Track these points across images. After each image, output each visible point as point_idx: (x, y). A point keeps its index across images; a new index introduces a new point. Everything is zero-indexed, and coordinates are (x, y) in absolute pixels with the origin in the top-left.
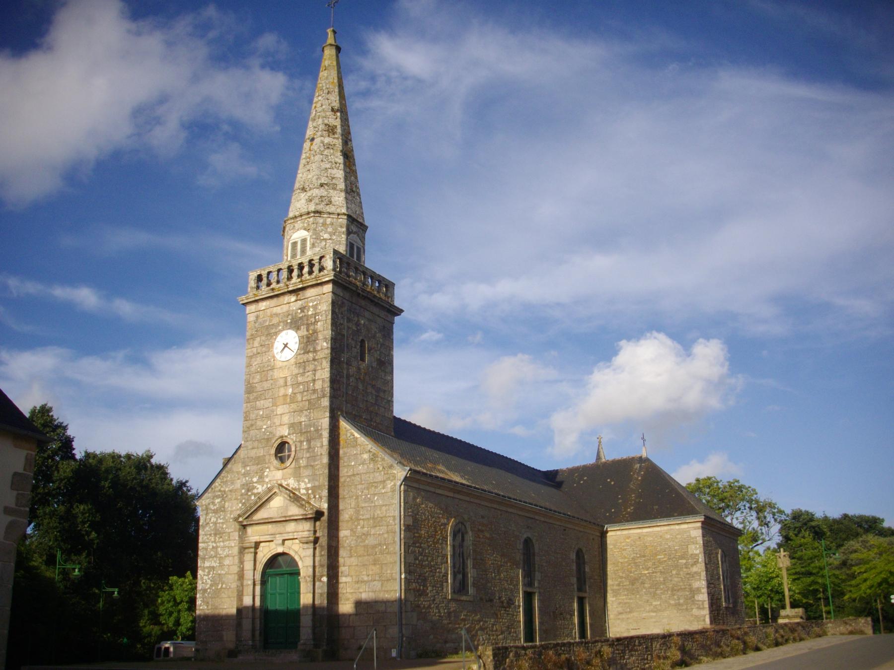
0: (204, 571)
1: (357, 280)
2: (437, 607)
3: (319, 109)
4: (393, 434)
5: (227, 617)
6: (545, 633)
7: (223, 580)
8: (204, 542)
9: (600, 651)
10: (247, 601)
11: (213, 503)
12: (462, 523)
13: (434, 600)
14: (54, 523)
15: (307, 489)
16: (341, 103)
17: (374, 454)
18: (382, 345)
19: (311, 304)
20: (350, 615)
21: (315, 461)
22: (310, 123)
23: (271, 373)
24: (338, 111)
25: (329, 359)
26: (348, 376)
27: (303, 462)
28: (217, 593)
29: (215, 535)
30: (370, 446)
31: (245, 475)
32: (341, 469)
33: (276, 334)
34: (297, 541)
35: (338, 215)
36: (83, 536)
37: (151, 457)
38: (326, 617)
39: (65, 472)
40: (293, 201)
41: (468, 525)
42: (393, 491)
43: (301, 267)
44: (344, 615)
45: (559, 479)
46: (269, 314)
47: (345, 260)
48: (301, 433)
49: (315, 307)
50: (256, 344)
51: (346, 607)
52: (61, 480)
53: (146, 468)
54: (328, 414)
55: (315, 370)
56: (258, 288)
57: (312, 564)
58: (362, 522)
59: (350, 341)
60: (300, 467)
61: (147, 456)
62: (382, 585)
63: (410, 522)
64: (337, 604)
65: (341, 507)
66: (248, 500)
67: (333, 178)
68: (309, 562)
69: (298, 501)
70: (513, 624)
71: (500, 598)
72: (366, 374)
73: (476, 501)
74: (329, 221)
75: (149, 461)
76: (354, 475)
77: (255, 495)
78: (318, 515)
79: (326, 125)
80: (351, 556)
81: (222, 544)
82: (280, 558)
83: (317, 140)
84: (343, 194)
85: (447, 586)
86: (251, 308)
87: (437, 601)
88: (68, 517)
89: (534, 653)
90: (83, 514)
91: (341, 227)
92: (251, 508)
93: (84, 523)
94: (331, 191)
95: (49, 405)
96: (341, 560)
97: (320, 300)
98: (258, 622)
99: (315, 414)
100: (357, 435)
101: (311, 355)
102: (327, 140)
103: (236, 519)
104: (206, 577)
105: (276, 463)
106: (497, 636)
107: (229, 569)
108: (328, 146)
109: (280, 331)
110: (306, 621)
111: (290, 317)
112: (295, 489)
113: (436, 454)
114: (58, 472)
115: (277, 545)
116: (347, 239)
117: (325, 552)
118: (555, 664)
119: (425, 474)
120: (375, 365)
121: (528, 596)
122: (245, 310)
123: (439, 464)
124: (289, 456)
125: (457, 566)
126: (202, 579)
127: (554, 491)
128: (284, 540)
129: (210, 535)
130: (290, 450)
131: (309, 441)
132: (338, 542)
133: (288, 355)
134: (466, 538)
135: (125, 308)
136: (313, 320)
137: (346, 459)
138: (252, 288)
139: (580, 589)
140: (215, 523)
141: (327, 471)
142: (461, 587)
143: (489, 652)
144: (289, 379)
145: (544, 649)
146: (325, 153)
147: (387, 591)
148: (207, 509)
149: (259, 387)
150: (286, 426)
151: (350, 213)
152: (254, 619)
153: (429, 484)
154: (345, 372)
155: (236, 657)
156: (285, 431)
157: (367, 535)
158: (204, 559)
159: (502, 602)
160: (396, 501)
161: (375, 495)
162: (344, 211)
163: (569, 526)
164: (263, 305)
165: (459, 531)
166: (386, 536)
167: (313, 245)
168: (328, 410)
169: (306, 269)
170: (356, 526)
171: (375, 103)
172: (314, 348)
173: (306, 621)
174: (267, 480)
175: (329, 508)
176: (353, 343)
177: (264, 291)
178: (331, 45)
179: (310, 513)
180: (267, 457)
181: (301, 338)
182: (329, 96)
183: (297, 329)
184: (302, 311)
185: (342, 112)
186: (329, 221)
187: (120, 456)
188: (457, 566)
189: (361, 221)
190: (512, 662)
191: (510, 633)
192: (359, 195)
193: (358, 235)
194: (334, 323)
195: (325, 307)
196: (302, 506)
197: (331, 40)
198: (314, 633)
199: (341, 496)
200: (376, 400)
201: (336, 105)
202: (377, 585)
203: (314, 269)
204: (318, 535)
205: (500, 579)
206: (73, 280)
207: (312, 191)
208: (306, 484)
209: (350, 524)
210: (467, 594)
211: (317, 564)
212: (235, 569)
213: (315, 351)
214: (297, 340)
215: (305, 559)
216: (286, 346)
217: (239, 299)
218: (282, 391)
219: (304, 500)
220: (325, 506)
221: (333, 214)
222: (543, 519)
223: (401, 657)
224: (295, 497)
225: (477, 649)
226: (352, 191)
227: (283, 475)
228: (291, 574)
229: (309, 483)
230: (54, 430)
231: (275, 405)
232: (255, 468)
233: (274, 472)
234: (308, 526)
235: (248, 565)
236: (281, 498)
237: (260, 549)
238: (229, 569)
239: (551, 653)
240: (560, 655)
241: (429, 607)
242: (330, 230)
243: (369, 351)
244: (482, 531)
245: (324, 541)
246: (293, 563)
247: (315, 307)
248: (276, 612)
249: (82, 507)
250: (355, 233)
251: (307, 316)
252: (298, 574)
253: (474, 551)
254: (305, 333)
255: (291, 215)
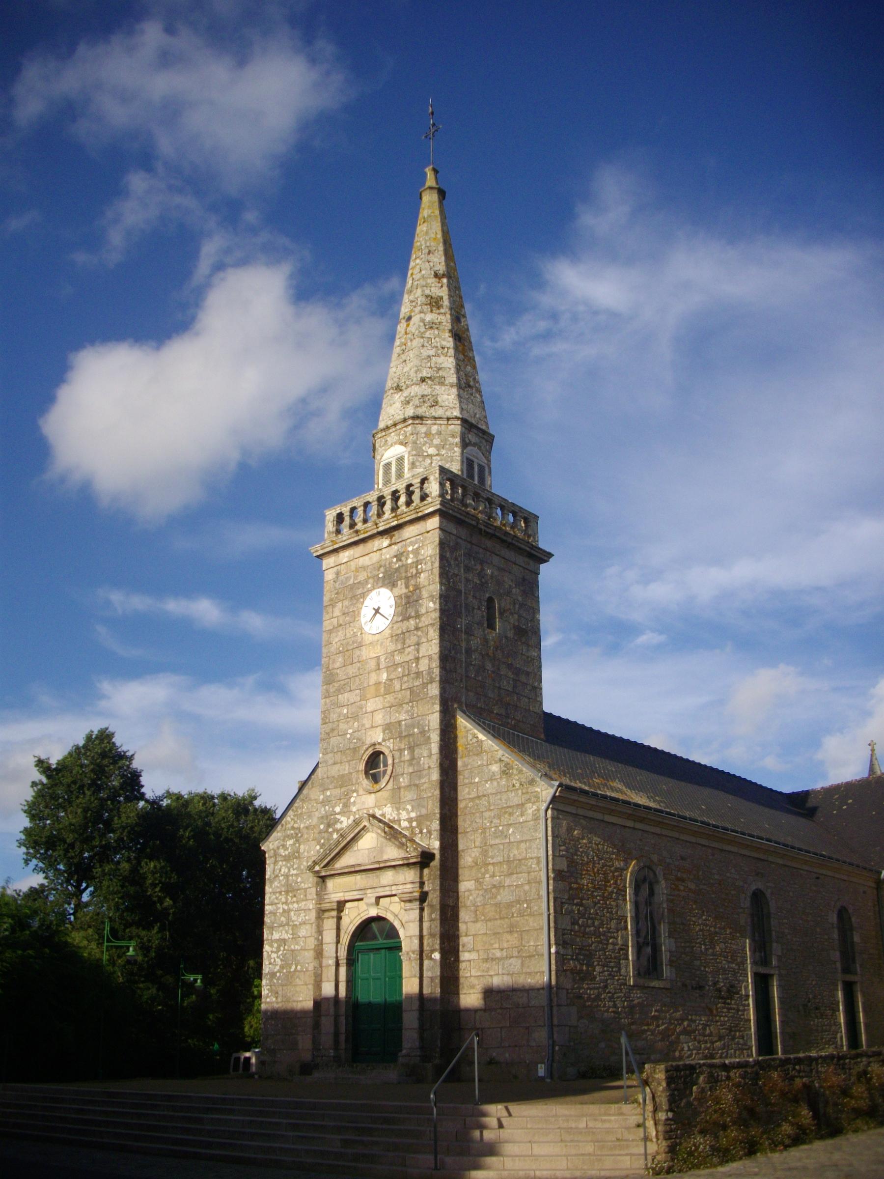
0: (272, 946)
1: (479, 510)
2: (611, 999)
3: (416, 277)
4: (542, 736)
5: (304, 1013)
6: (793, 1039)
7: (298, 960)
8: (272, 904)
9: (865, 1072)
10: (328, 990)
11: (284, 846)
12: (649, 868)
13: (606, 987)
14: (115, 885)
15: (410, 820)
16: (447, 265)
17: (507, 764)
18: (522, 605)
19: (410, 549)
20: (476, 1011)
21: (420, 777)
22: (406, 296)
23: (357, 652)
24: (443, 276)
25: (437, 626)
26: (469, 651)
27: (404, 781)
28: (290, 978)
29: (287, 892)
30: (501, 752)
31: (324, 803)
32: (459, 788)
33: (364, 595)
34: (396, 899)
35: (448, 419)
36: (155, 903)
37: (255, 798)
38: (441, 1013)
39: (128, 817)
40: (384, 406)
41: (659, 870)
42: (536, 819)
43: (395, 495)
44: (467, 1010)
45: (810, 803)
46: (353, 568)
47: (458, 481)
48: (401, 737)
49: (416, 552)
50: (337, 612)
51: (470, 998)
52: (124, 828)
53: (246, 811)
54: (437, 707)
55: (418, 644)
56: (338, 532)
57: (417, 933)
58: (491, 868)
59: (470, 599)
60: (399, 788)
61: (250, 796)
62: (522, 964)
63: (563, 865)
64: (457, 994)
65: (461, 847)
66: (328, 840)
67: (439, 369)
68: (414, 929)
69: (396, 838)
70: (737, 1025)
71: (715, 984)
72: (496, 648)
73: (671, 834)
74: (434, 429)
75: (251, 803)
76: (479, 797)
77: (337, 831)
78: (426, 858)
79: (427, 296)
80: (476, 921)
81: (296, 905)
82: (374, 925)
83: (416, 319)
84: (454, 391)
85: (627, 966)
86: (328, 562)
87: (611, 988)
88: (135, 878)
89: (743, 1077)
90: (153, 873)
91: (453, 436)
92: (331, 850)
93: (154, 885)
94: (437, 387)
95: (111, 729)
96: (462, 927)
97: (424, 541)
98: (343, 1020)
99: (420, 709)
100: (481, 737)
101: (412, 622)
102: (429, 317)
103: (310, 868)
104: (274, 955)
105: (366, 783)
106: (713, 1043)
107: (305, 942)
108: (431, 326)
109: (370, 591)
110: (410, 1020)
111: (382, 569)
112: (394, 821)
113: (611, 766)
114: (120, 818)
115: (368, 905)
116: (462, 453)
117: (436, 915)
118: (783, 1094)
119: (583, 792)
120: (510, 634)
121: (762, 982)
122: (321, 566)
123: (614, 780)
124: (385, 772)
125: (643, 934)
126: (269, 956)
127: (802, 820)
128: (378, 898)
129: (280, 893)
130: (386, 765)
131: (411, 749)
132: (457, 898)
133: (381, 624)
134: (656, 891)
135: (255, 622)
136: (414, 571)
137: (466, 773)
138: (329, 533)
139: (847, 969)
140: (287, 876)
141: (437, 792)
142: (650, 967)
143: (660, 1075)
144: (382, 659)
145: (762, 1068)
146: (427, 335)
147: (530, 974)
148: (276, 855)
149: (341, 674)
150: (380, 729)
151: (466, 416)
152: (337, 1017)
153: (592, 808)
154: (464, 644)
155: (310, 1074)
156: (377, 736)
157: (499, 887)
158: (272, 928)
159: (719, 990)
160: (541, 835)
161: (510, 825)
162: (457, 413)
163: (824, 872)
164: (345, 556)
165: (644, 880)
166: (527, 887)
167: (413, 465)
168: (438, 702)
169: (403, 499)
170: (484, 874)
171: (559, 347)
172: (417, 612)
173: (410, 1020)
174: (354, 809)
175: (442, 848)
176: (476, 603)
177: (347, 535)
178: (431, 188)
179: (413, 855)
180: (354, 775)
181: (398, 598)
182: (432, 257)
183: (392, 585)
184: (399, 560)
185: (449, 277)
186: (434, 429)
187: (213, 797)
188: (643, 934)
189: (484, 427)
190: (703, 1090)
191: (733, 1038)
192: (479, 391)
193: (480, 448)
194: (445, 574)
195: (430, 550)
196: (402, 845)
197: (430, 181)
198: (422, 1038)
199: (460, 830)
200: (515, 687)
201: (441, 268)
202: (515, 964)
203: (413, 497)
204: (426, 888)
205: (713, 954)
206: (189, 589)
207: (409, 390)
208: (408, 813)
209: (474, 870)
210: (659, 977)
211: (425, 933)
212: (312, 943)
213: (418, 616)
214: (392, 601)
215: (407, 924)
216: (377, 611)
217: (312, 549)
218: (373, 678)
219: (405, 836)
220: (435, 845)
221: (440, 418)
222: (781, 861)
223: (552, 1078)
224: (391, 832)
225: (641, 1070)
226: (467, 385)
227: (377, 801)
228: (390, 949)
229: (411, 809)
230: (115, 762)
231: (363, 698)
232: (337, 792)
233: (364, 798)
234: (411, 875)
235: (329, 936)
236: (374, 835)
237: (346, 911)
238: (305, 942)
239: (775, 1075)
240: (792, 1078)
241: (598, 998)
242: (436, 441)
243: (501, 614)
244: (682, 880)
245: (434, 898)
246: (392, 933)
247: (416, 552)
248: (370, 1005)
249: (152, 865)
250: (474, 445)
251: (406, 567)
252: (400, 948)
253: (671, 910)
254: (404, 591)
255: (382, 425)
